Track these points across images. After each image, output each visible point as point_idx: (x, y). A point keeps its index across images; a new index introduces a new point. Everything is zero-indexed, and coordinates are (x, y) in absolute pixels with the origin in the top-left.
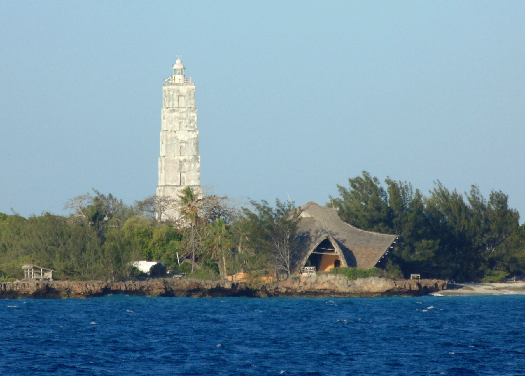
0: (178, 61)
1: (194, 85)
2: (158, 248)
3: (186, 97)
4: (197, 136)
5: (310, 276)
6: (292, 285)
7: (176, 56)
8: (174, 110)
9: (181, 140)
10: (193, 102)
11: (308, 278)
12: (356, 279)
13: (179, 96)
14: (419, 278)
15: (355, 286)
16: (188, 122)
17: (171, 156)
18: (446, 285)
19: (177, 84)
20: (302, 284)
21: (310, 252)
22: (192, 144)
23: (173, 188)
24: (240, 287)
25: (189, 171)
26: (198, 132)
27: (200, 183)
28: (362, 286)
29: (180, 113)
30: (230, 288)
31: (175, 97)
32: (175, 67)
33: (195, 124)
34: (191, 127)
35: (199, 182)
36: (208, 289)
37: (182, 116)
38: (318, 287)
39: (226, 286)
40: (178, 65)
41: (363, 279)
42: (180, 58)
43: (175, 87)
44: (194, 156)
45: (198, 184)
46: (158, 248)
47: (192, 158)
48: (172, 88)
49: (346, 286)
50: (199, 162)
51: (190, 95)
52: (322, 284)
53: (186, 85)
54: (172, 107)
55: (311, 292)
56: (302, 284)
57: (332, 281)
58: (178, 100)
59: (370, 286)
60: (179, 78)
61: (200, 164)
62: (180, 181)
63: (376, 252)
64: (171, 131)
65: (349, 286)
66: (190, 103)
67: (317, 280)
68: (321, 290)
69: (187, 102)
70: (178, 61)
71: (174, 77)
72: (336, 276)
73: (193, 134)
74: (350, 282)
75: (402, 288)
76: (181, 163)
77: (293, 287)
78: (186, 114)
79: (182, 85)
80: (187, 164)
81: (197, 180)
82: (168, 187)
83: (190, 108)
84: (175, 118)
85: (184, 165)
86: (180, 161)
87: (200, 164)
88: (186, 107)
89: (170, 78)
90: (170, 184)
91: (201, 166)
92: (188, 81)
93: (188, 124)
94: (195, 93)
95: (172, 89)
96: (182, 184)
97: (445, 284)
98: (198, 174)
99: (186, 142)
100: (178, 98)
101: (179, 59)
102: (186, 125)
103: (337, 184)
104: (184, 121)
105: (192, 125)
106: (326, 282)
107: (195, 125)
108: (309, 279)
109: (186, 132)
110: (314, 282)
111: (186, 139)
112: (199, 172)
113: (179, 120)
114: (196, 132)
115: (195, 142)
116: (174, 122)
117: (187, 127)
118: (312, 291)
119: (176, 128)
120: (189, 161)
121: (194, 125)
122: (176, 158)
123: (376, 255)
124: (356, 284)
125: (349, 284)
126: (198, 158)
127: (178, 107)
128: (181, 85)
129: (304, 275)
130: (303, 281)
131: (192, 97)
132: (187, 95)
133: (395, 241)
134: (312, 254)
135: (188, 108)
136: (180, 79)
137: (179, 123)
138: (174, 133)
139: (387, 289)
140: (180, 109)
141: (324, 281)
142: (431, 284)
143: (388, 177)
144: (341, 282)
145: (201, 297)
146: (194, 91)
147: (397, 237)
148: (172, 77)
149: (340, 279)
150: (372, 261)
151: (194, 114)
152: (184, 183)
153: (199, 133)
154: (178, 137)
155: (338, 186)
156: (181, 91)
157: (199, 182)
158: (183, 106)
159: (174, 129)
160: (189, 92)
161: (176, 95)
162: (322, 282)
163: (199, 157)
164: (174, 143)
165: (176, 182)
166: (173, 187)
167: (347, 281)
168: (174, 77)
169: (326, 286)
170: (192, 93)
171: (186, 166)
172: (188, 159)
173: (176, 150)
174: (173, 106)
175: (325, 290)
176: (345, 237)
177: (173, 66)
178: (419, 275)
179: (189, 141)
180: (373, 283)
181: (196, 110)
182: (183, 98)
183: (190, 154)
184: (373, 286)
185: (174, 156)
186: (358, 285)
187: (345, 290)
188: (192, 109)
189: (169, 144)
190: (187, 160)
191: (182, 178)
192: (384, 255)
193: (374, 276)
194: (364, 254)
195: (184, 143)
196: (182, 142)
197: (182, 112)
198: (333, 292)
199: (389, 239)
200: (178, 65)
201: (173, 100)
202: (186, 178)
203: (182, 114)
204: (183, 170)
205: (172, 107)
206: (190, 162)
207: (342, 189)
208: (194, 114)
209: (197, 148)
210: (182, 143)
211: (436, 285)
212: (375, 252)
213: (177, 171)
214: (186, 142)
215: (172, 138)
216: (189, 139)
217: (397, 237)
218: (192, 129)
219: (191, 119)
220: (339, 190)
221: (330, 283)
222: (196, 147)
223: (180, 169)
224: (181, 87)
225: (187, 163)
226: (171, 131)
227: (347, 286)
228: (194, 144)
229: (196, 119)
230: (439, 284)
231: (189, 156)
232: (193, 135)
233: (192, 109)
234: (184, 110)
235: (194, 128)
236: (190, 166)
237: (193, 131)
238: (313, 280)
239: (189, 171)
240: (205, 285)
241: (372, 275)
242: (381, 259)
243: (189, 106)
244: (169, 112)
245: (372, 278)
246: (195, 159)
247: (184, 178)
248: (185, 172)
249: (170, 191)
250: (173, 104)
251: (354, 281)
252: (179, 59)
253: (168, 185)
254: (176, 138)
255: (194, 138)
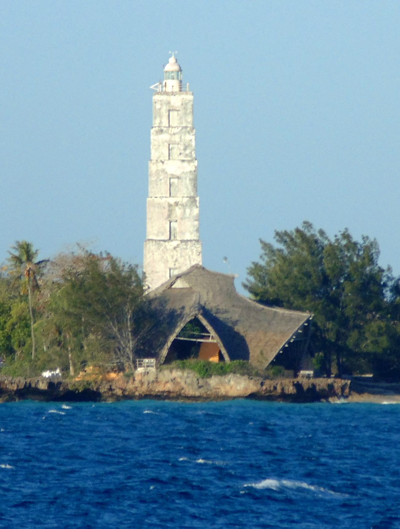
0: (172, 60)
1: (193, 94)
2: (19, 331)
3: (179, 112)
4: (194, 169)
5: (148, 373)
6: (125, 385)
7: (170, 52)
8: (162, 131)
9: (172, 175)
10: (190, 119)
11: (144, 376)
12: (210, 376)
13: (169, 111)
14: (310, 377)
15: (208, 387)
16: (182, 147)
17: (156, 197)
18: (348, 386)
19: (167, 93)
20: (137, 383)
21: (172, 338)
22: (188, 181)
23: (158, 244)
24: (64, 389)
25: (182, 219)
26: (196, 163)
27: (199, 237)
28: (218, 387)
29: (171, 135)
30: (46, 388)
31: (164, 112)
32: (168, 68)
33: (193, 151)
34: (186, 155)
35: (198, 234)
36: (13, 390)
37: (173, 139)
38: (159, 388)
39: (41, 385)
40: (171, 66)
41: (219, 377)
42: (175, 55)
43: (164, 98)
44: (190, 197)
45: (196, 238)
46: (19, 331)
47: (188, 201)
48: (160, 99)
49: (196, 386)
50: (197, 207)
51: (185, 109)
52: (165, 384)
53: (180, 95)
54: (159, 127)
55: (150, 395)
56: (137, 383)
57: (179, 380)
58: (169, 115)
59: (228, 387)
60: (172, 85)
61: (198, 209)
62: (168, 233)
63: (277, 338)
64: (157, 161)
65: (200, 387)
66: (186, 121)
67: (157, 378)
68: (163, 392)
69: (181, 119)
70: (172, 60)
71: (166, 83)
72: (183, 373)
73: (189, 165)
74: (201, 382)
75: (270, 391)
76: (171, 208)
77: (128, 388)
78: (179, 136)
79: (173, 94)
80: (180, 209)
81: (195, 233)
82: (151, 242)
83: (186, 127)
84: (163, 143)
85: (175, 210)
86: (170, 205)
87: (198, 209)
88: (179, 127)
89: (158, 84)
90: (154, 238)
91: (200, 211)
92: (183, 89)
93: (182, 152)
94: (193, 105)
95: (158, 101)
96: (172, 238)
97: (346, 384)
98: (196, 223)
99: (178, 178)
100: (168, 113)
101: (173, 56)
102: (179, 152)
103: (260, 239)
104: (176, 146)
105: (188, 152)
106: (170, 381)
107: (193, 152)
108: (146, 377)
109: (179, 163)
110: (153, 381)
111: (178, 173)
112: (196, 220)
113: (169, 145)
114: (194, 162)
115: (191, 177)
116: (161, 147)
117: (182, 155)
118: (152, 393)
119: (164, 157)
120: (182, 205)
121: (191, 153)
122: (164, 199)
123: (277, 342)
124: (209, 385)
125: (200, 384)
126: (195, 201)
127: (168, 125)
128: (172, 94)
129: (140, 370)
130: (138, 378)
131: (188, 111)
132: (181, 109)
133: (306, 322)
134: (175, 340)
135: (183, 128)
136: (173, 86)
137: (169, 150)
138: (161, 164)
139: (249, 392)
140: (170, 128)
141: (167, 380)
142: (321, 385)
143: (340, 231)
144: (189, 381)
145: (7, 401)
146: (191, 103)
147: (310, 317)
148: (161, 83)
149: (188, 377)
150: (272, 351)
151: (193, 138)
152: (175, 237)
153: (198, 163)
154: (166, 170)
155: (261, 242)
156: (172, 103)
157: (198, 234)
158: (175, 125)
159: (162, 159)
160: (184, 105)
161: (164, 109)
162: (164, 382)
163: (198, 199)
164: (161, 178)
165: (163, 234)
166: (158, 242)
167: (198, 380)
168: (166, 83)
169: (169, 386)
170: (189, 107)
171: (178, 211)
172: (182, 202)
173: (164, 188)
174: (161, 125)
175: (169, 392)
176: (236, 317)
177: (164, 66)
178: (311, 372)
179: (183, 176)
180: (232, 383)
181: (194, 131)
182: (175, 113)
183: (184, 194)
184: (231, 388)
185: (160, 197)
186: (212, 386)
187: (194, 393)
188: (189, 129)
189: (154, 179)
190: (180, 203)
191: (172, 229)
192: (289, 343)
193: (235, 373)
194: (261, 340)
195: (175, 178)
196: (173, 177)
197: (174, 134)
198: (179, 396)
199: (299, 320)
200: (171, 66)
201: (161, 117)
202: (178, 230)
203: (173, 136)
204: (173, 218)
205: (159, 127)
206: (184, 206)
207: (266, 246)
208: (190, 138)
209: (195, 187)
210: (173, 178)
211: (331, 386)
212: (276, 338)
213: (165, 219)
214: (178, 178)
215: (158, 172)
216: (183, 172)
217: (310, 317)
218: (189, 159)
219: (187, 144)
220: (263, 248)
221: (174, 383)
222: (193, 184)
223: (169, 216)
224: (172, 97)
225: (180, 207)
226: (157, 161)
227: (197, 387)
228: (190, 180)
229: (193, 143)
230: (336, 385)
231: (183, 197)
232: (191, 167)
233: (189, 129)
234: (176, 130)
235: (191, 156)
236: (185, 212)
237: (189, 161)
238: (151, 378)
239: (182, 219)
240: (10, 384)
241: (231, 372)
242: (284, 349)
243: (184, 125)
244: (155, 133)
245: (231, 376)
246: (192, 202)
247: (175, 229)
248: (176, 221)
249: (154, 247)
250: (161, 122)
251: (208, 380)
252: (173, 56)
253: (152, 240)
254: (163, 171)
255: (191, 172)
